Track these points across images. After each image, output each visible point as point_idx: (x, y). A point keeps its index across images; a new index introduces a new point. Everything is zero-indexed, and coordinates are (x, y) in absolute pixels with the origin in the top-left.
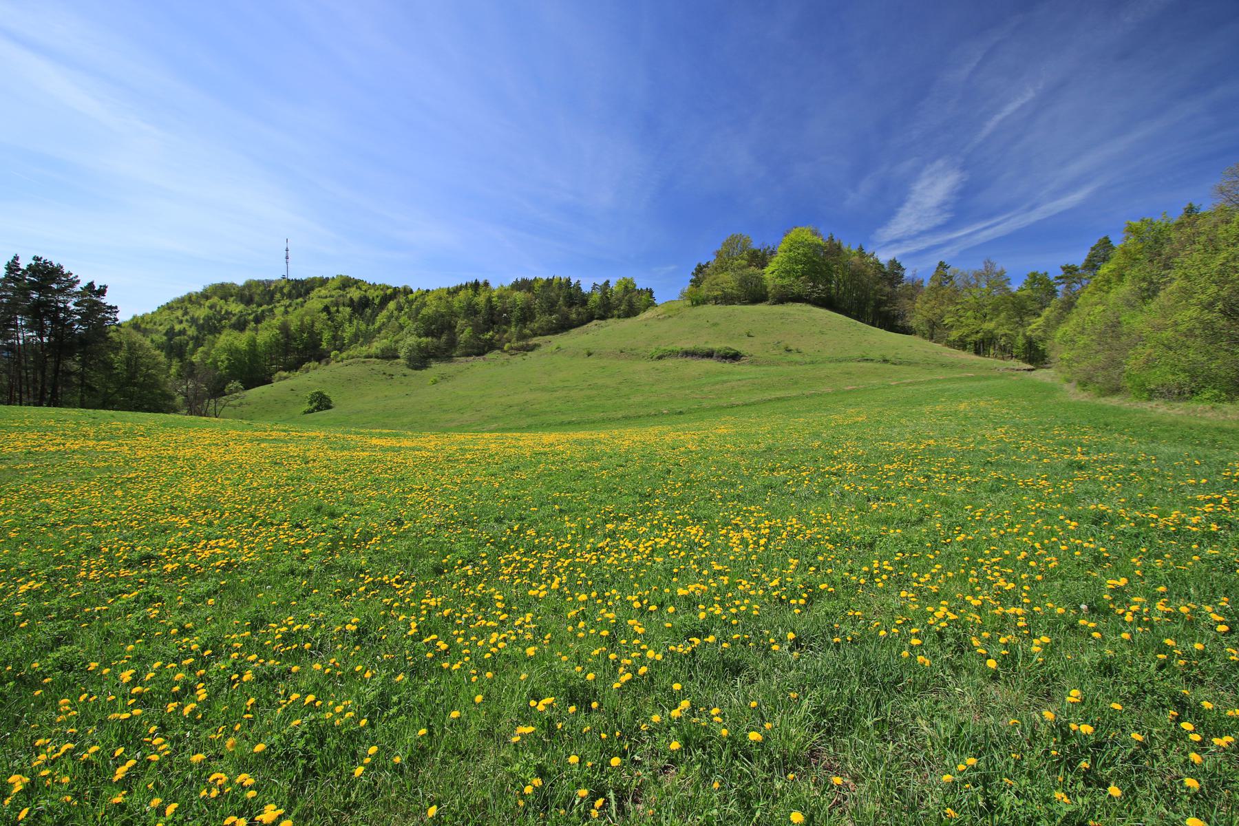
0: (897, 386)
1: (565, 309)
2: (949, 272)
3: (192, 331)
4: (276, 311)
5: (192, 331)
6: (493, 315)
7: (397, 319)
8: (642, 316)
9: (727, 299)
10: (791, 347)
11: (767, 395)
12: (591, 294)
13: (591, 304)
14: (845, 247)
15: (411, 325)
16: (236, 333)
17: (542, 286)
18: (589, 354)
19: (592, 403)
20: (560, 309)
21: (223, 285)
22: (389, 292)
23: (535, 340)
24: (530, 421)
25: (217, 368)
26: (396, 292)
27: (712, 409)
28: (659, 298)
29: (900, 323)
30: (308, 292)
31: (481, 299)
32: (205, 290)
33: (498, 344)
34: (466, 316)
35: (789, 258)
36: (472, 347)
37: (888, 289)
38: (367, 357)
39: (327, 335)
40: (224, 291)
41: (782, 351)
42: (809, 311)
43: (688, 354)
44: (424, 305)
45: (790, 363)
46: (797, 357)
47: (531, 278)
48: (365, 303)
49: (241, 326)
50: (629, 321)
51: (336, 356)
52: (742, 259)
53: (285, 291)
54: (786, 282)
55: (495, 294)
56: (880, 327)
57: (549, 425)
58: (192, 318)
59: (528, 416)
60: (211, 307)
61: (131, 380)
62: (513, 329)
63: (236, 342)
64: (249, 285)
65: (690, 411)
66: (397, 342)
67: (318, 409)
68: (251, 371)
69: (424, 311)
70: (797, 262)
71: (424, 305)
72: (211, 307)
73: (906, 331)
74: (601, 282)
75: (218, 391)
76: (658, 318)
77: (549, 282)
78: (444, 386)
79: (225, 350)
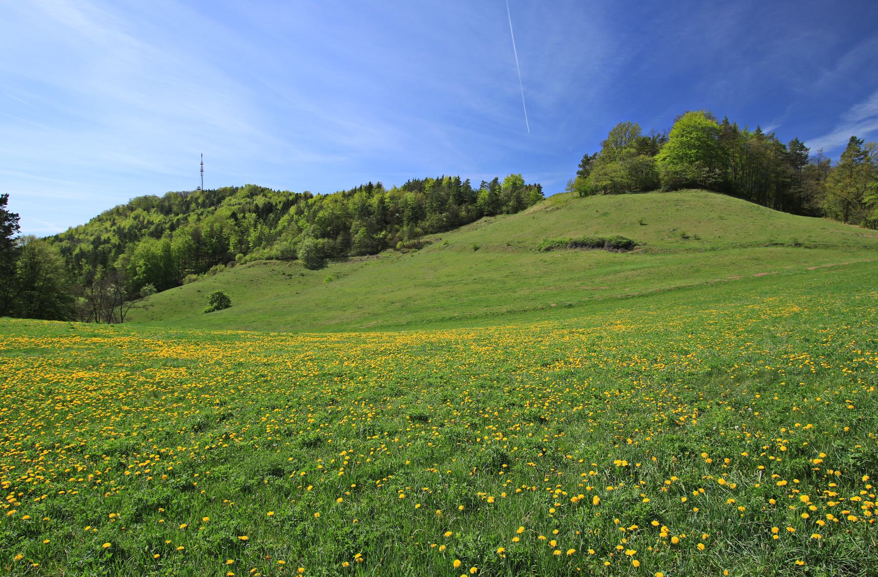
0: (817, 270)
1: (455, 207)
2: (862, 148)
3: (115, 240)
4: (190, 219)
5: (115, 240)
6: (386, 215)
7: (297, 222)
8: (530, 210)
9: (616, 189)
10: (688, 234)
11: (665, 285)
12: (478, 192)
13: (480, 201)
14: (741, 130)
15: (310, 228)
16: (153, 240)
17: (433, 186)
18: (476, 249)
19: (475, 298)
20: (451, 207)
21: (146, 198)
22: (291, 198)
23: (426, 238)
24: (410, 317)
25: (135, 274)
26: (298, 197)
27: (604, 301)
28: (547, 192)
29: (806, 206)
30: (219, 201)
31: (374, 201)
32: (131, 203)
33: (391, 243)
34: (360, 217)
35: (681, 142)
36: (366, 246)
37: (791, 171)
38: (268, 259)
39: (233, 240)
40: (146, 203)
41: (679, 238)
42: (706, 197)
43: (576, 244)
44: (321, 208)
45: (688, 250)
46: (695, 244)
47: (422, 178)
48: (268, 208)
49: (157, 234)
50: (521, 214)
51: (240, 258)
52: (631, 146)
53: (200, 201)
54: (678, 168)
55: (388, 195)
56: (784, 210)
57: (430, 322)
58: (119, 228)
59: (410, 312)
60: (135, 218)
61: (29, 284)
62: (405, 228)
63: (152, 249)
64: (168, 197)
65: (581, 304)
66: (295, 244)
67: (218, 308)
68: (164, 275)
69: (320, 214)
70: (694, 146)
71: (321, 208)
72: (135, 218)
73: (815, 213)
74: (489, 179)
75: (135, 294)
76: (546, 211)
77: (439, 182)
78: (337, 285)
79: (142, 256)
